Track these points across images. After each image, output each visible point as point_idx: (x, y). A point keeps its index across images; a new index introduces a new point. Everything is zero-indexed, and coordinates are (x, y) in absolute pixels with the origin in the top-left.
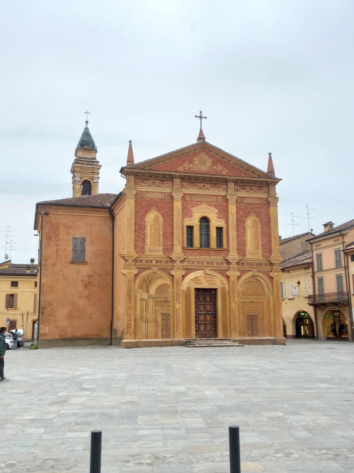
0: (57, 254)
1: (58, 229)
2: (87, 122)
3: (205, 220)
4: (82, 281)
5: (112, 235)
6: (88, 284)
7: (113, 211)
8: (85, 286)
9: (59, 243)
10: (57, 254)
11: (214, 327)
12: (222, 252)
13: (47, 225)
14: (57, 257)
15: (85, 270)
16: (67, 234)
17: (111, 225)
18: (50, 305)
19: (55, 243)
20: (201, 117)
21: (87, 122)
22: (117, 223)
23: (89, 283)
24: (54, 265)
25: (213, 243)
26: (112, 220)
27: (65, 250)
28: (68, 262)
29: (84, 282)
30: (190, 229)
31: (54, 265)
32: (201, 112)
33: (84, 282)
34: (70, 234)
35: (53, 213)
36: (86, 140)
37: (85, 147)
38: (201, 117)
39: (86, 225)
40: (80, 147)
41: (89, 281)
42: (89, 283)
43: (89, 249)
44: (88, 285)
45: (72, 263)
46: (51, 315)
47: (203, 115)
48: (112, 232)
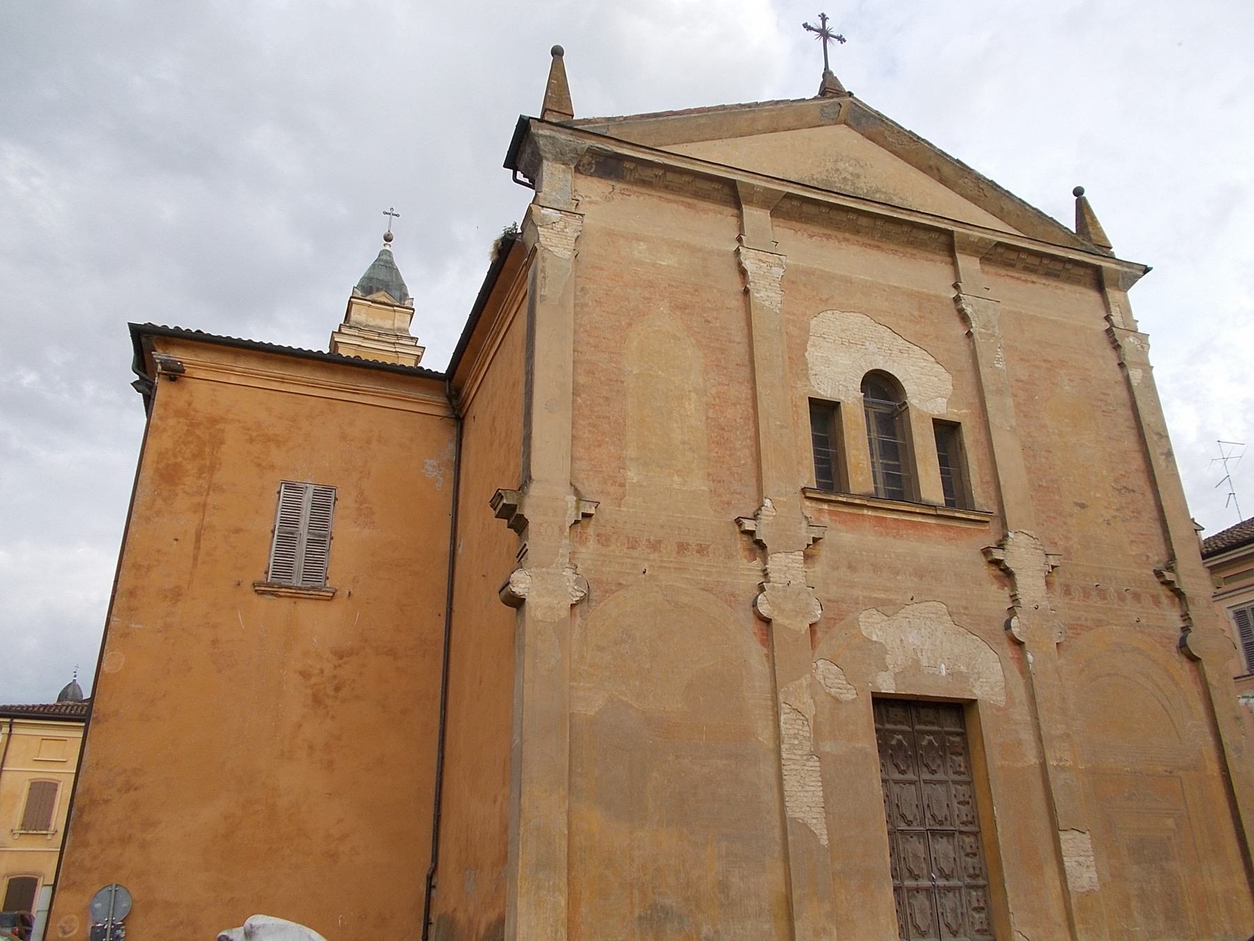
0: (197, 548)
1: (218, 442)
2: (388, 239)
3: (880, 386)
4: (305, 675)
5: (451, 487)
6: (331, 692)
7: (458, 391)
8: (317, 700)
9: (213, 499)
10: (197, 548)
11: (978, 910)
12: (951, 527)
13: (172, 422)
14: (195, 558)
15: (320, 625)
16: (259, 465)
17: (452, 447)
18: (128, 787)
19: (196, 499)
20: (825, 34)
21: (388, 239)
22: (470, 439)
23: (337, 689)
24: (176, 595)
25: (931, 486)
26: (455, 431)
27: (238, 531)
28: (247, 585)
29: (313, 680)
30: (824, 413)
31: (176, 595)
32: (824, 18)
33: (313, 680)
34: (272, 467)
35: (202, 375)
36: (381, 277)
37: (374, 296)
38: (825, 34)
39: (343, 437)
40: (359, 294)
41: (335, 677)
42: (337, 689)
43: (347, 533)
44: (328, 696)
45: (261, 589)
46: (125, 840)
47: (833, 26)
48: (451, 474)
